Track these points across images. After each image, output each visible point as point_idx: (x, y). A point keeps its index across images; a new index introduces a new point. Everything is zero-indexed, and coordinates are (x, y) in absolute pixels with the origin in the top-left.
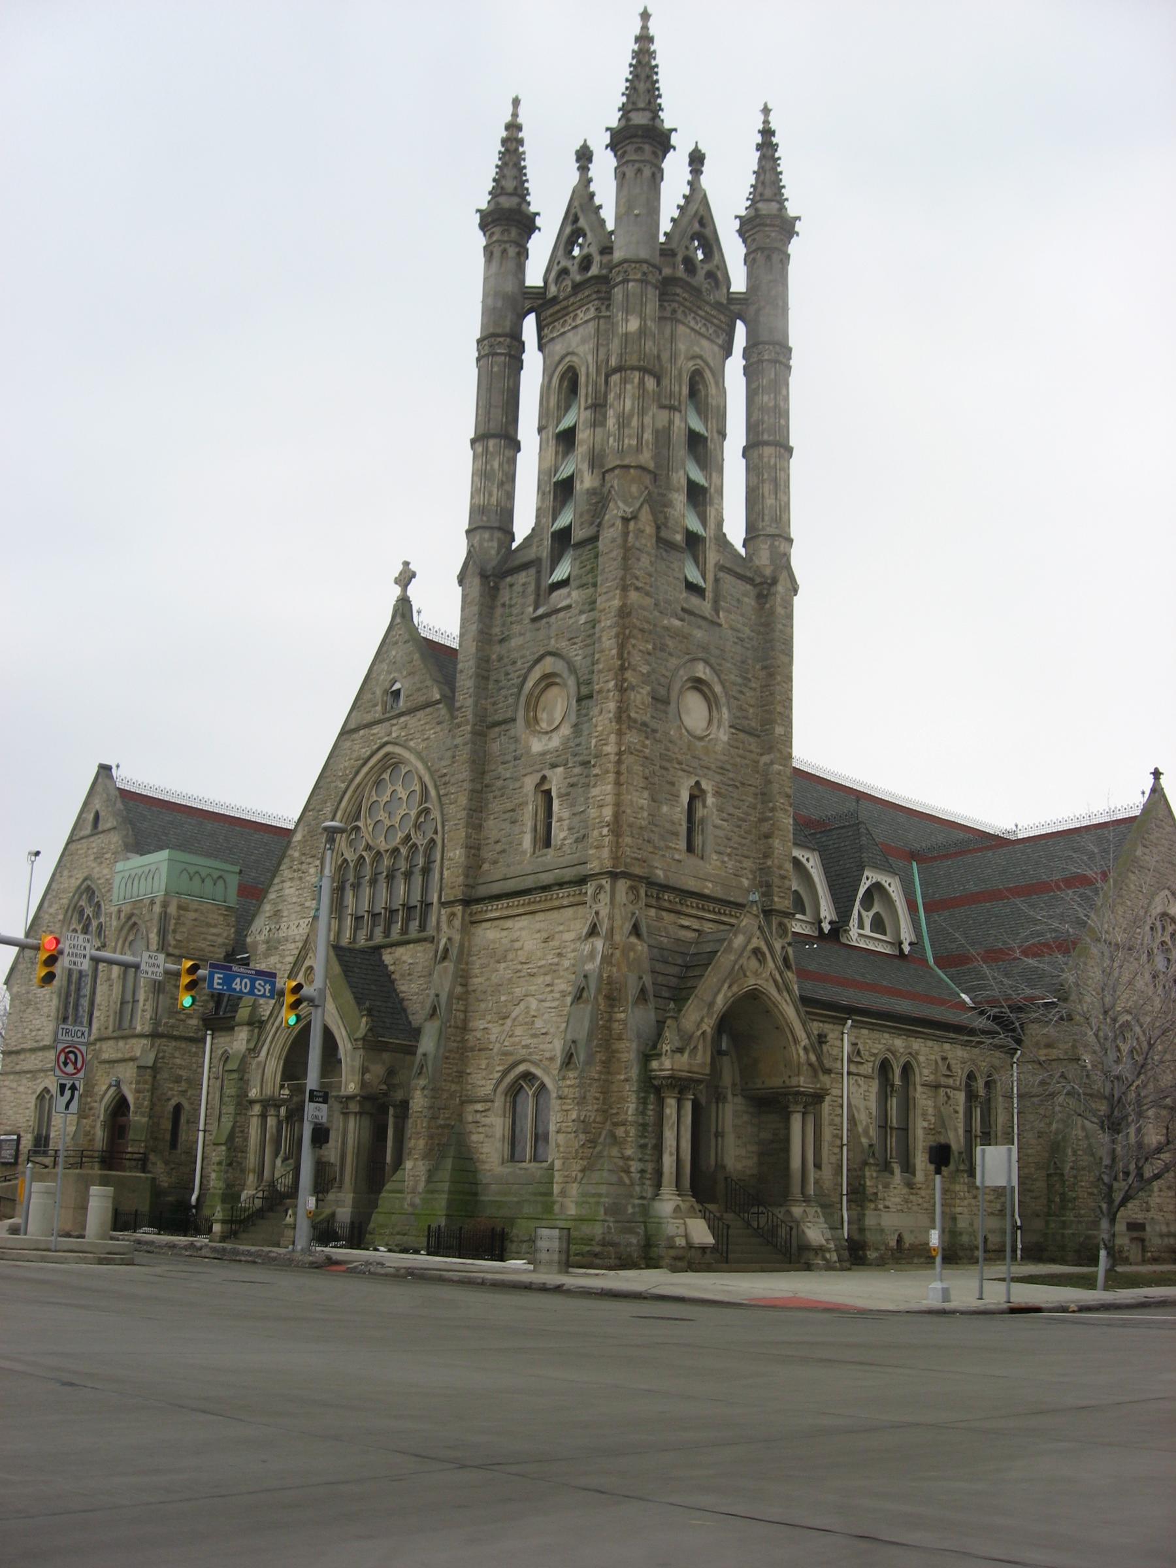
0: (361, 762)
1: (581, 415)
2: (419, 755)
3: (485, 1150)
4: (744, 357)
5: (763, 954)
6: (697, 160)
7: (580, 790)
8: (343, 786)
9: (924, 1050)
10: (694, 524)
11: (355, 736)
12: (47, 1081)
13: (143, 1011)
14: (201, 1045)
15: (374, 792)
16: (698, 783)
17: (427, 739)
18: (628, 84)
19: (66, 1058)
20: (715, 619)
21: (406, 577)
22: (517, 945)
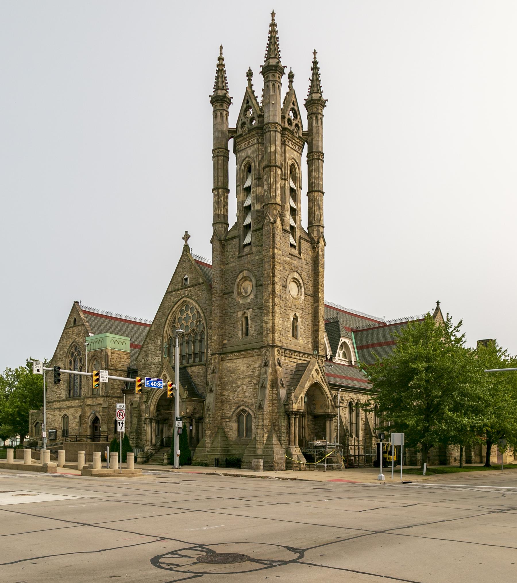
0: (175, 303)
1: (253, 181)
2: (196, 302)
3: (230, 434)
4: (307, 157)
5: (318, 371)
6: (291, 76)
7: (258, 318)
8: (169, 311)
9: (362, 398)
10: (293, 223)
11: (172, 294)
12: (65, 412)
13: (102, 388)
14: (122, 399)
15: (179, 314)
16: (295, 314)
17: (199, 296)
18: (268, 46)
19: (120, 414)
20: (300, 257)
21: (187, 237)
22: (238, 368)
